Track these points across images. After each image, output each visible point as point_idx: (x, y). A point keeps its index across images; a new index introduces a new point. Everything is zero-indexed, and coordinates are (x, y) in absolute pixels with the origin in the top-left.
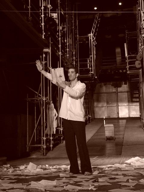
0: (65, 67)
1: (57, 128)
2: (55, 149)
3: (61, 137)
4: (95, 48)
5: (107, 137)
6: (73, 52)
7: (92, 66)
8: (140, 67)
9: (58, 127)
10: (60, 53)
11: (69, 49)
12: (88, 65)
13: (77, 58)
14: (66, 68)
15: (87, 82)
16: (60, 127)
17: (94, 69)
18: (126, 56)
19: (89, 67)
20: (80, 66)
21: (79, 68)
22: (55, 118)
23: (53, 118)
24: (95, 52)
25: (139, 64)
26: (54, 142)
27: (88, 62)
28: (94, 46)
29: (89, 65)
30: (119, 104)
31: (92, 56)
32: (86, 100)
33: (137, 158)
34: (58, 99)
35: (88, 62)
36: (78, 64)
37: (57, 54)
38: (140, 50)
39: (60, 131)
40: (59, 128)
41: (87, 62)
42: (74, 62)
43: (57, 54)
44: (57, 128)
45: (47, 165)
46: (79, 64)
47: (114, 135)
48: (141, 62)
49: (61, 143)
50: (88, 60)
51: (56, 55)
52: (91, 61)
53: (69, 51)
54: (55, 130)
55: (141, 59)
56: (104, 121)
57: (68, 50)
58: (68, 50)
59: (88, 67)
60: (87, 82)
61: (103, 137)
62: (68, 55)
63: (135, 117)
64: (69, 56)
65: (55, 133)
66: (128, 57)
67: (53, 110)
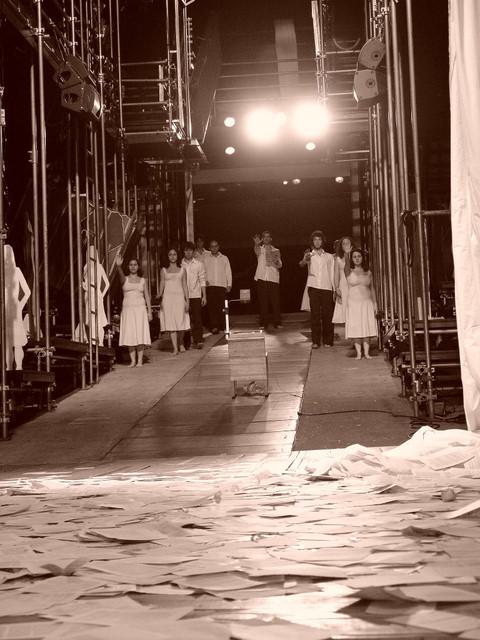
0: (64, 92)
1: (30, 350)
2: (19, 432)
3: (48, 384)
4: (188, 20)
5: (235, 382)
6: (94, 33)
7: (175, 93)
8: (373, 96)
9: (32, 343)
10: (40, 29)
11: (76, 14)
12: (161, 92)
13: (114, 61)
14: (66, 96)
15: (155, 162)
16: (42, 344)
17: (184, 108)
18: (317, 54)
19: (166, 98)
20: (126, 93)
21: (123, 102)
22: (21, 305)
23: (14, 306)
24: (188, 37)
25: (371, 84)
26: (14, 405)
27: (161, 76)
28: (185, 11)
29: (166, 92)
30: (163, 330)
31: (178, 51)
32: (151, 240)
33: (355, 449)
34: (31, 230)
35: (161, 76)
36: (117, 86)
37: (27, 32)
38: (375, 26)
39: (44, 359)
40: (37, 349)
41: (158, 78)
42: (101, 74)
43: (26, 33)
44: (30, 350)
45: (351, 213)
46: (123, 83)
47: (265, 377)
48: (378, 76)
49: (45, 410)
50: (160, 68)
51: (23, 39)
52: (174, 74)
53: (77, 26)
54: (19, 356)
55: (376, 63)
56: (227, 316)
57: (73, 18)
58: (73, 18)
59: (161, 99)
60: (155, 162)
61: (220, 385)
62: (74, 43)
63: (328, 451)
64: (78, 48)
65: (19, 367)
66: (323, 56)
67: (13, 271)
